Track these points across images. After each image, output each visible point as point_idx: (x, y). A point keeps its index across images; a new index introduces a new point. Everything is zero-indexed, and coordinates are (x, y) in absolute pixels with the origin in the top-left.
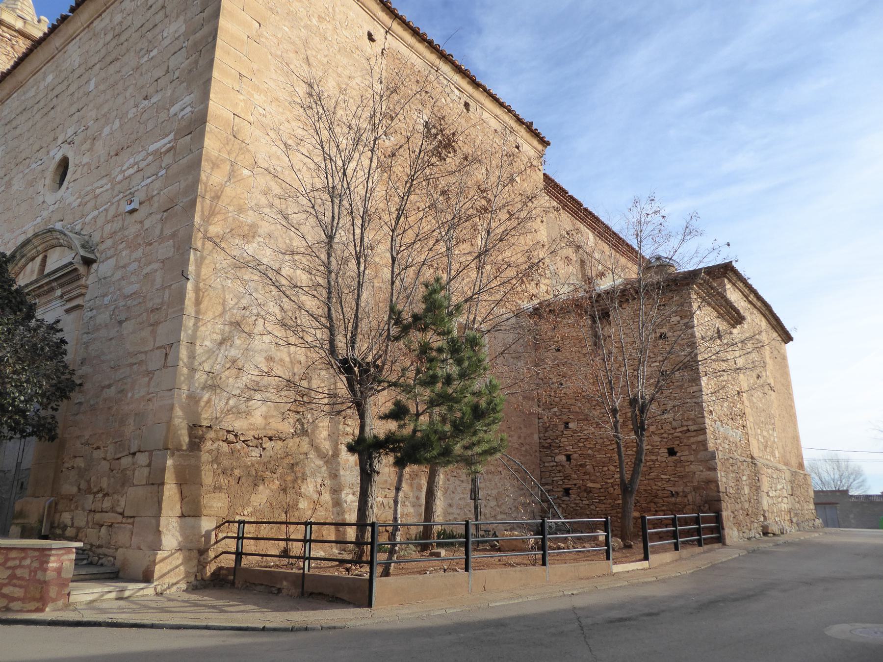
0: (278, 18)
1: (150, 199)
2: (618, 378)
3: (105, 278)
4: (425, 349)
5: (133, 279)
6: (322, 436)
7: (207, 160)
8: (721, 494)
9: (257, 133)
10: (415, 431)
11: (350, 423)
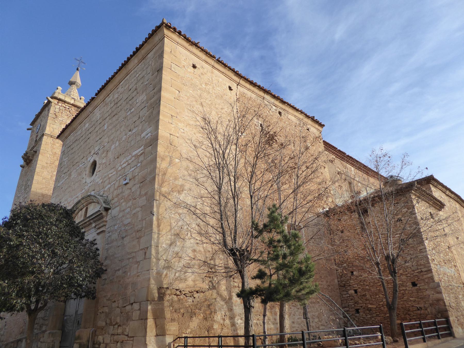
0: (187, 87)
1: (134, 177)
2: (377, 245)
3: (115, 217)
4: (271, 242)
5: (128, 216)
6: (223, 289)
7: (159, 157)
8: (447, 307)
9: (181, 141)
10: (270, 284)
11: (236, 281)
